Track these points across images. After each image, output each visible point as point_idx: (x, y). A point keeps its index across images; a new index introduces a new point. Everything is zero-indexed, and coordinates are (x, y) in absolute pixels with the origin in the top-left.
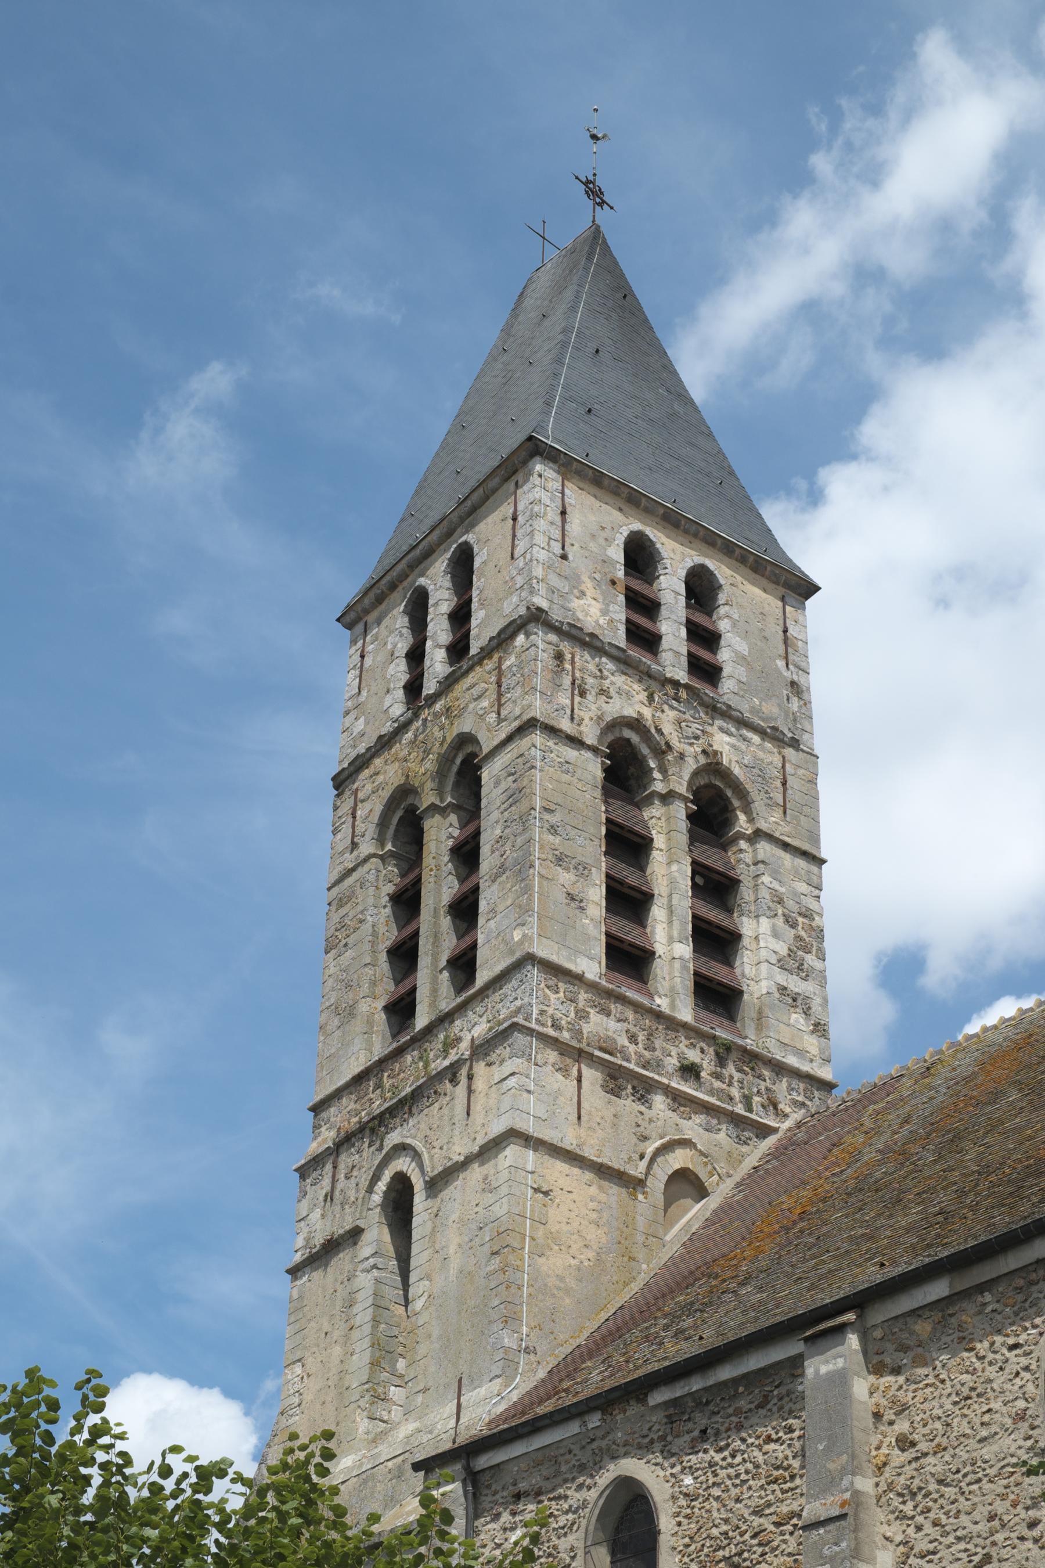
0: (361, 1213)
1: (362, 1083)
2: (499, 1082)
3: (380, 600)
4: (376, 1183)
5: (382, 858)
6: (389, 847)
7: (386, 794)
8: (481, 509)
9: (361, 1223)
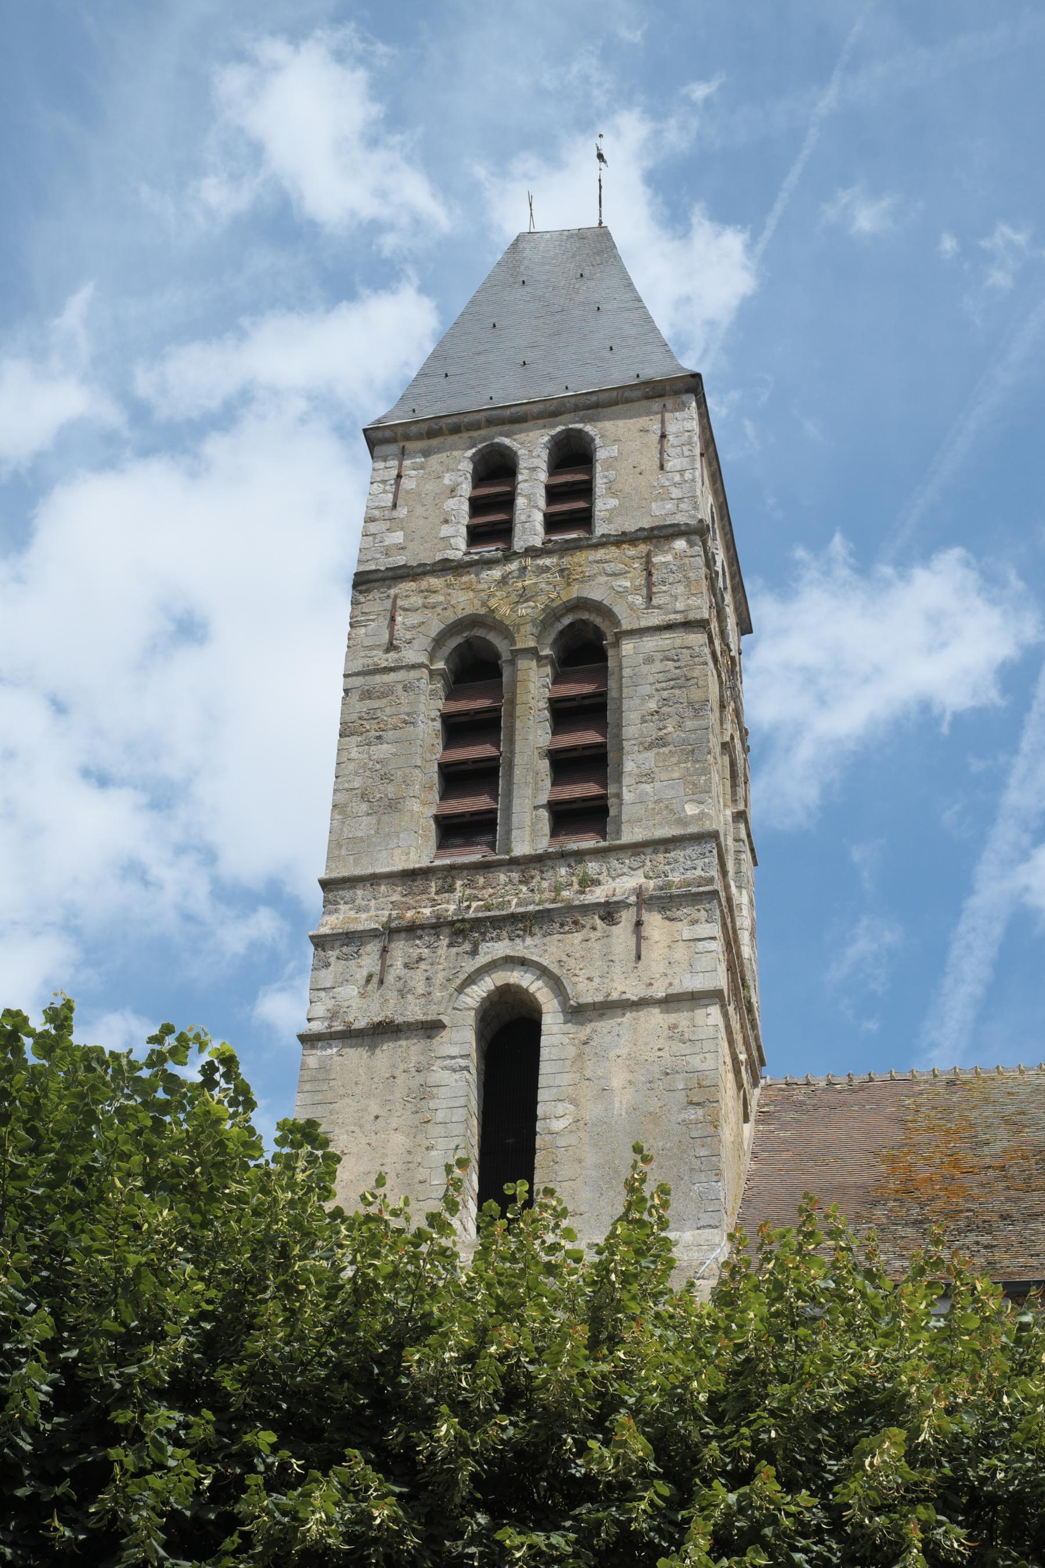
0: (446, 1009)
1: (415, 880)
2: (690, 940)
3: (456, 430)
4: (468, 985)
5: (432, 673)
6: (440, 665)
7: (451, 617)
8: (605, 410)
9: (445, 1019)
